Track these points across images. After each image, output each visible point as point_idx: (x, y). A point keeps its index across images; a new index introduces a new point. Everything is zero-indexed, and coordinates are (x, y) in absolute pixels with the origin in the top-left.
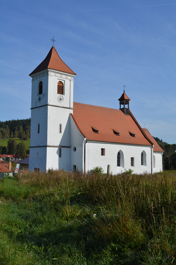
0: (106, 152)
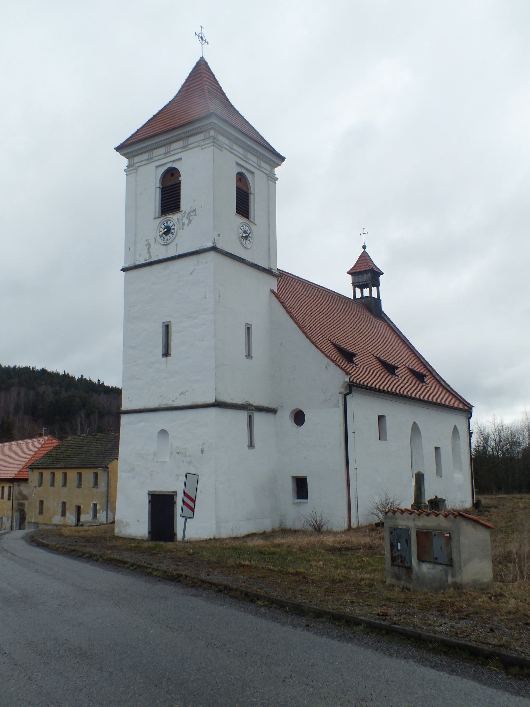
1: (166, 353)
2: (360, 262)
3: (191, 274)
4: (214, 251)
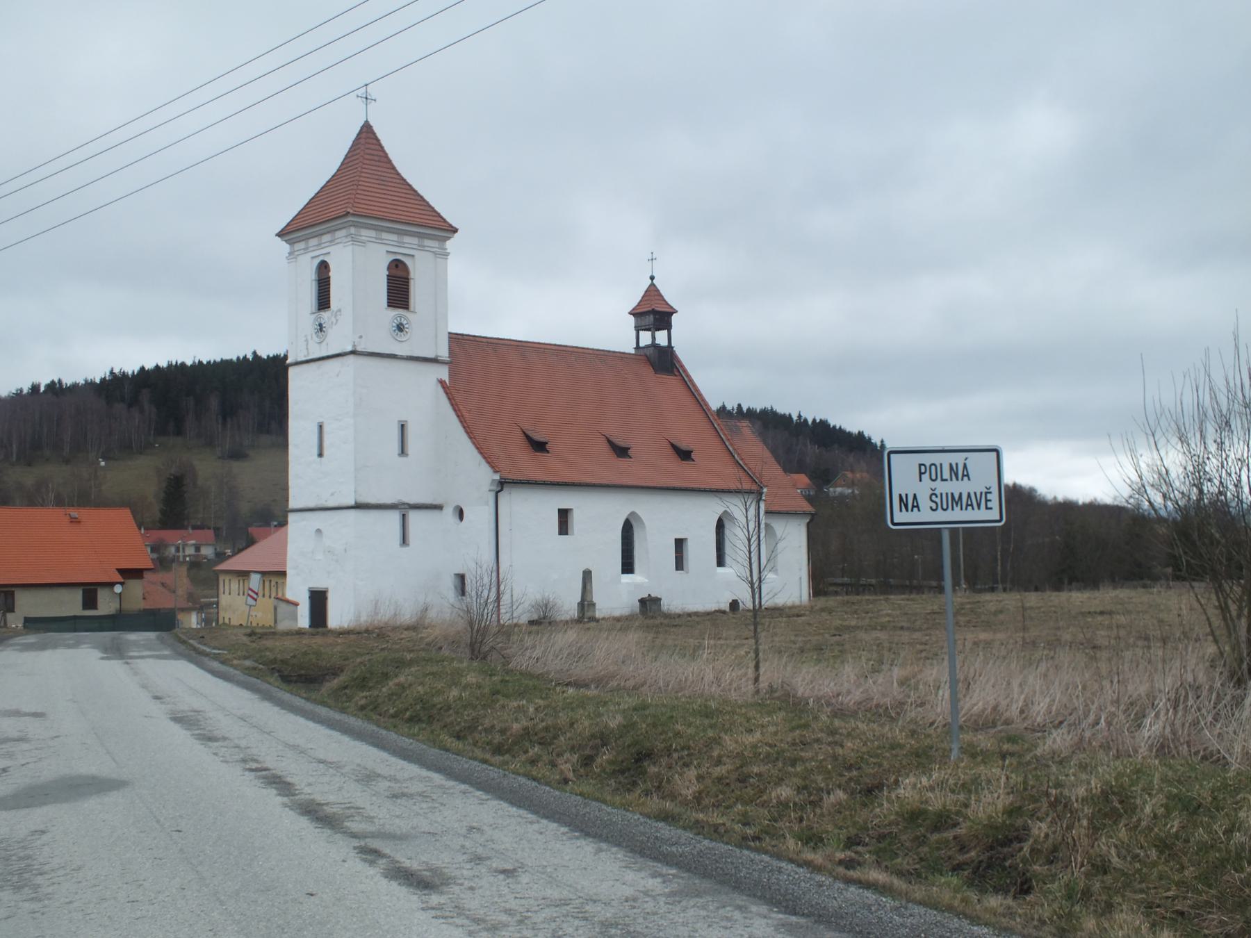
0: (576, 520)
1: (320, 455)
2: (646, 298)
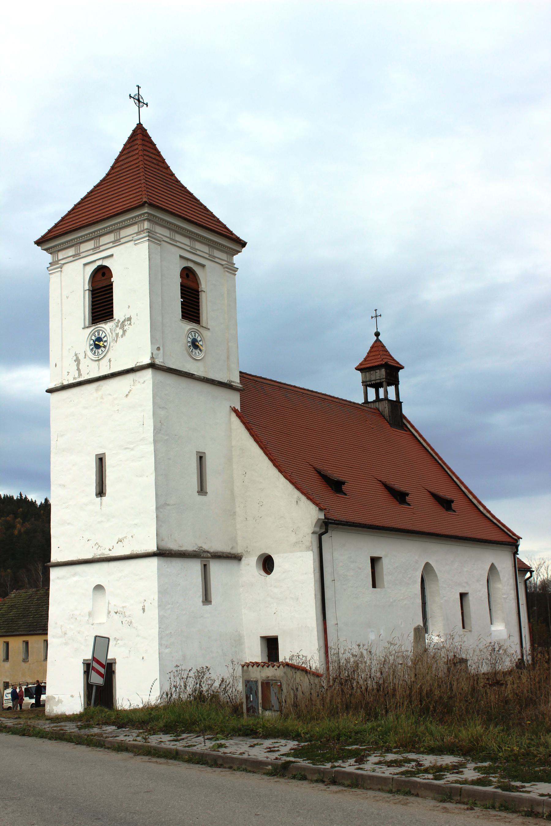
1: (101, 492)
2: (372, 354)
3: (127, 395)
4: (152, 368)
